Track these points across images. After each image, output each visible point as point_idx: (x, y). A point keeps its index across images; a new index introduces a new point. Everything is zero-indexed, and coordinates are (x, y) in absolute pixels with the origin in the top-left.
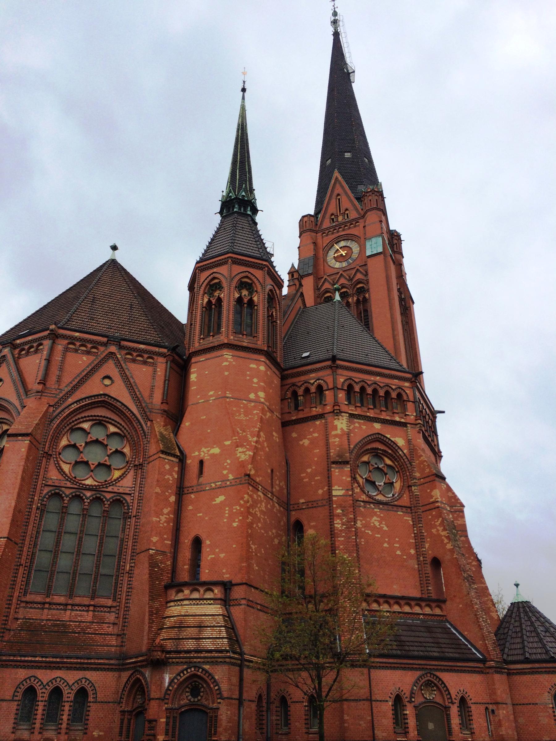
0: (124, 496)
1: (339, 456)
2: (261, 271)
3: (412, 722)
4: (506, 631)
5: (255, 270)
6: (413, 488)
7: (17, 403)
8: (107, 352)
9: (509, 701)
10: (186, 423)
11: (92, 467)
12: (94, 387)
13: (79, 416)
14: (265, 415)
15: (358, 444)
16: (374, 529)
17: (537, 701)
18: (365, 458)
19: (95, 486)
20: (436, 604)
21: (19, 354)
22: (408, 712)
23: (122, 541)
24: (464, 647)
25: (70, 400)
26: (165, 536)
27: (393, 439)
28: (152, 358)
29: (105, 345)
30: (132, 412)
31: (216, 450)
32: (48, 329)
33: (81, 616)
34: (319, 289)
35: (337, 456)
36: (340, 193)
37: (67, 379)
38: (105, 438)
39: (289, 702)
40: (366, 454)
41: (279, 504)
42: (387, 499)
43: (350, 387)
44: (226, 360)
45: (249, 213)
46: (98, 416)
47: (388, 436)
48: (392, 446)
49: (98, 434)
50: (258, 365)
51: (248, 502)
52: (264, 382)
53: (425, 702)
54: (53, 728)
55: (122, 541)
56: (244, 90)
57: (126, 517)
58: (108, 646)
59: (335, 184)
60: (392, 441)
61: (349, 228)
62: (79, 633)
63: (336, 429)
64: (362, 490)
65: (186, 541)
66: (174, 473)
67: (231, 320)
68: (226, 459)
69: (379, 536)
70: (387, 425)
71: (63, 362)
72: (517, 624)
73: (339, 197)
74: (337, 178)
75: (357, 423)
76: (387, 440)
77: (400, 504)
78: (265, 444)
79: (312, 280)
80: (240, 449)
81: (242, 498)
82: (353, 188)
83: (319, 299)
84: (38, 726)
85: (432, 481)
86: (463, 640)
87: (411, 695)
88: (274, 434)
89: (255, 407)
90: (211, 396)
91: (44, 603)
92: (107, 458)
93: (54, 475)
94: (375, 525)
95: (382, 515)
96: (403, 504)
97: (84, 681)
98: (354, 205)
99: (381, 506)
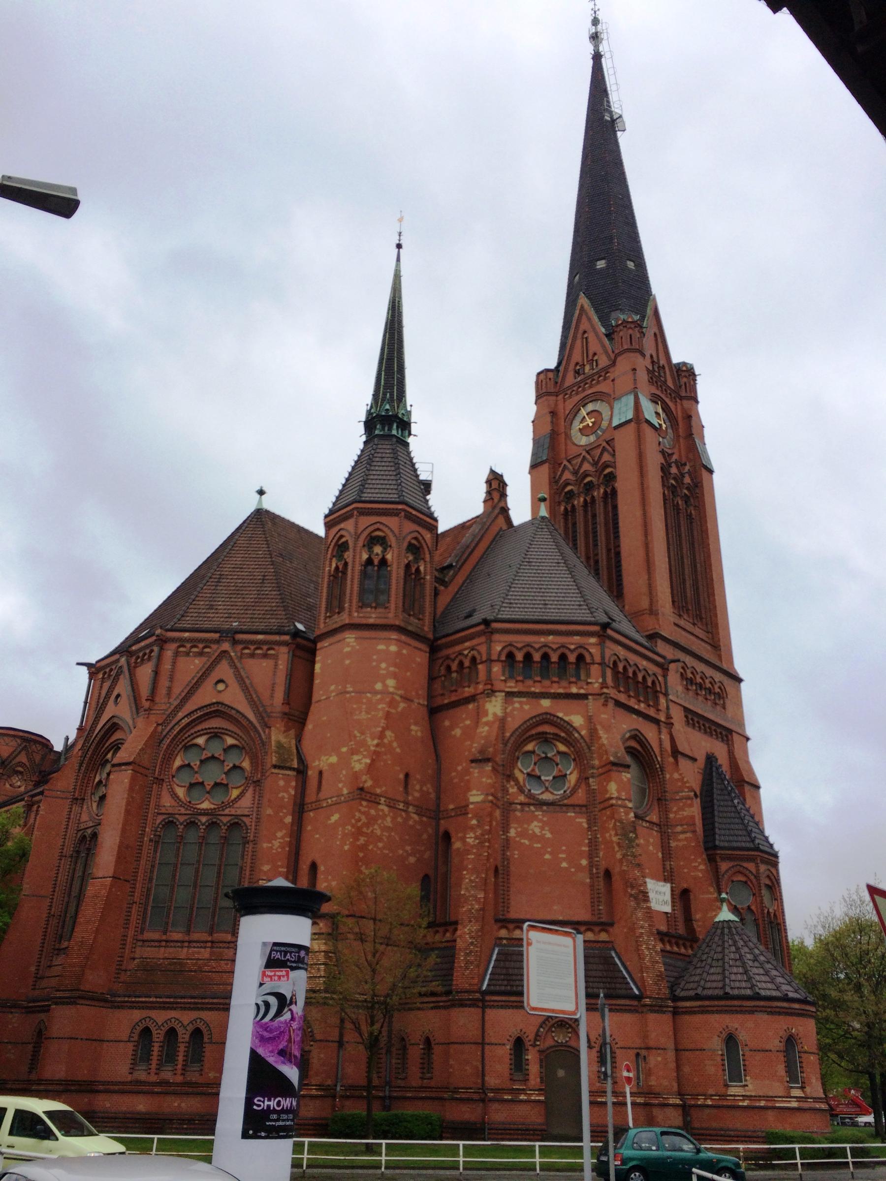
1: (482, 751)
3: (534, 1069)
4: (704, 957)
5: (389, 518)
6: (591, 780)
8: (219, 651)
9: (671, 1045)
10: (309, 726)
11: (208, 788)
12: (205, 696)
13: (192, 731)
14: (396, 708)
15: (517, 729)
16: (533, 837)
18: (530, 747)
19: (211, 809)
20: (600, 928)
21: (136, 663)
22: (529, 1057)
23: (242, 868)
24: (621, 980)
25: (180, 715)
26: (279, 863)
27: (566, 718)
28: (273, 649)
29: (217, 642)
31: (334, 759)
32: (153, 635)
33: (199, 953)
34: (557, 482)
39: (433, 1043)
40: (530, 741)
41: (418, 814)
42: (555, 797)
43: (511, 656)
44: (348, 645)
45: (394, 432)
47: (560, 715)
48: (567, 727)
49: (215, 748)
52: (395, 665)
54: (170, 1069)
55: (242, 868)
57: (246, 842)
59: (580, 315)
60: (565, 721)
61: (598, 382)
62: (195, 971)
63: (487, 715)
64: (521, 790)
69: (539, 845)
70: (560, 701)
72: (719, 949)
73: (586, 335)
74: (582, 307)
75: (517, 703)
76: (559, 721)
79: (547, 470)
80: (356, 757)
81: (353, 817)
82: (604, 319)
84: (154, 1066)
85: (607, 772)
89: (380, 701)
90: (332, 691)
91: (160, 941)
93: (167, 801)
94: (534, 832)
95: (545, 819)
96: (577, 802)
98: (603, 346)
99: (545, 808)
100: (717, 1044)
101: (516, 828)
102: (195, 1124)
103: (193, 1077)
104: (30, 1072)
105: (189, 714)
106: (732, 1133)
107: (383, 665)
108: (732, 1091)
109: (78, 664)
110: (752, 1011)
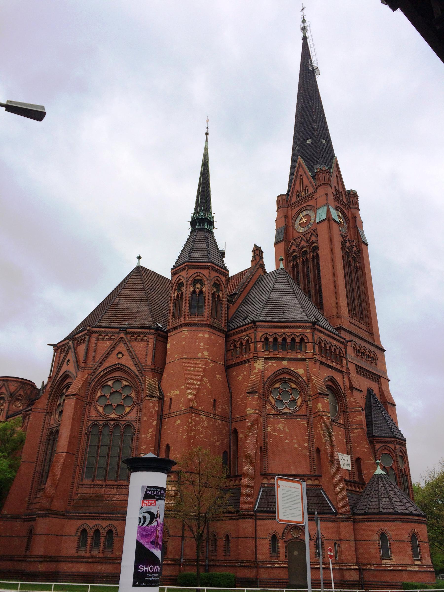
0: (132, 422)
1: (253, 388)
2: (207, 270)
3: (282, 550)
6: (309, 402)
7: (75, 374)
8: (119, 338)
9: (352, 538)
10: (165, 375)
11: (114, 407)
12: (112, 360)
16: (280, 432)
17: (370, 539)
18: (277, 385)
19: (116, 418)
20: (315, 478)
21: (77, 344)
22: (280, 545)
23: (131, 448)
28: (146, 336)
29: (118, 333)
30: (134, 372)
31: (177, 392)
32: (86, 329)
33: (110, 491)
34: (288, 251)
35: (251, 388)
36: (302, 174)
37: (99, 357)
38: (121, 389)
43: (266, 339)
44: (184, 334)
45: (206, 227)
46: (116, 377)
47: (292, 369)
48: (296, 375)
50: (204, 334)
51: (191, 424)
52: (208, 345)
53: (292, 539)
55: (131, 448)
56: (207, 134)
57: (133, 435)
58: (123, 507)
61: (308, 201)
62: (108, 500)
64: (273, 407)
65: (163, 447)
66: (155, 408)
67: (187, 307)
68: (182, 397)
71: (96, 348)
73: (302, 177)
74: (300, 163)
77: (299, 414)
78: (208, 385)
80: (188, 391)
81: (188, 422)
82: (311, 169)
83: (289, 258)
86: (328, 501)
87: (283, 535)
88: (217, 376)
90: (176, 358)
92: (122, 401)
93: (93, 414)
96: (301, 414)
97: (111, 526)
98: (311, 182)
100: (376, 538)
101: (271, 427)
102: (109, 578)
103: (109, 554)
104: (26, 552)
105: (104, 370)
106: (385, 584)
107: (202, 344)
108: (384, 562)
109: (48, 345)
110: (393, 521)
